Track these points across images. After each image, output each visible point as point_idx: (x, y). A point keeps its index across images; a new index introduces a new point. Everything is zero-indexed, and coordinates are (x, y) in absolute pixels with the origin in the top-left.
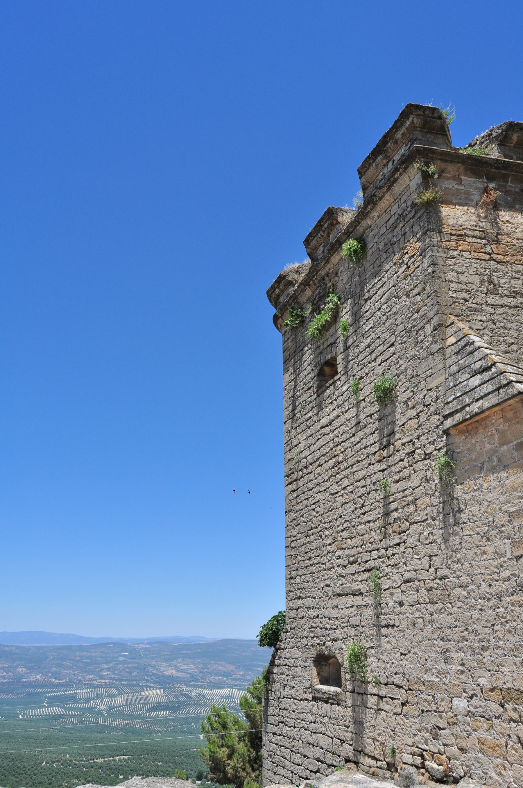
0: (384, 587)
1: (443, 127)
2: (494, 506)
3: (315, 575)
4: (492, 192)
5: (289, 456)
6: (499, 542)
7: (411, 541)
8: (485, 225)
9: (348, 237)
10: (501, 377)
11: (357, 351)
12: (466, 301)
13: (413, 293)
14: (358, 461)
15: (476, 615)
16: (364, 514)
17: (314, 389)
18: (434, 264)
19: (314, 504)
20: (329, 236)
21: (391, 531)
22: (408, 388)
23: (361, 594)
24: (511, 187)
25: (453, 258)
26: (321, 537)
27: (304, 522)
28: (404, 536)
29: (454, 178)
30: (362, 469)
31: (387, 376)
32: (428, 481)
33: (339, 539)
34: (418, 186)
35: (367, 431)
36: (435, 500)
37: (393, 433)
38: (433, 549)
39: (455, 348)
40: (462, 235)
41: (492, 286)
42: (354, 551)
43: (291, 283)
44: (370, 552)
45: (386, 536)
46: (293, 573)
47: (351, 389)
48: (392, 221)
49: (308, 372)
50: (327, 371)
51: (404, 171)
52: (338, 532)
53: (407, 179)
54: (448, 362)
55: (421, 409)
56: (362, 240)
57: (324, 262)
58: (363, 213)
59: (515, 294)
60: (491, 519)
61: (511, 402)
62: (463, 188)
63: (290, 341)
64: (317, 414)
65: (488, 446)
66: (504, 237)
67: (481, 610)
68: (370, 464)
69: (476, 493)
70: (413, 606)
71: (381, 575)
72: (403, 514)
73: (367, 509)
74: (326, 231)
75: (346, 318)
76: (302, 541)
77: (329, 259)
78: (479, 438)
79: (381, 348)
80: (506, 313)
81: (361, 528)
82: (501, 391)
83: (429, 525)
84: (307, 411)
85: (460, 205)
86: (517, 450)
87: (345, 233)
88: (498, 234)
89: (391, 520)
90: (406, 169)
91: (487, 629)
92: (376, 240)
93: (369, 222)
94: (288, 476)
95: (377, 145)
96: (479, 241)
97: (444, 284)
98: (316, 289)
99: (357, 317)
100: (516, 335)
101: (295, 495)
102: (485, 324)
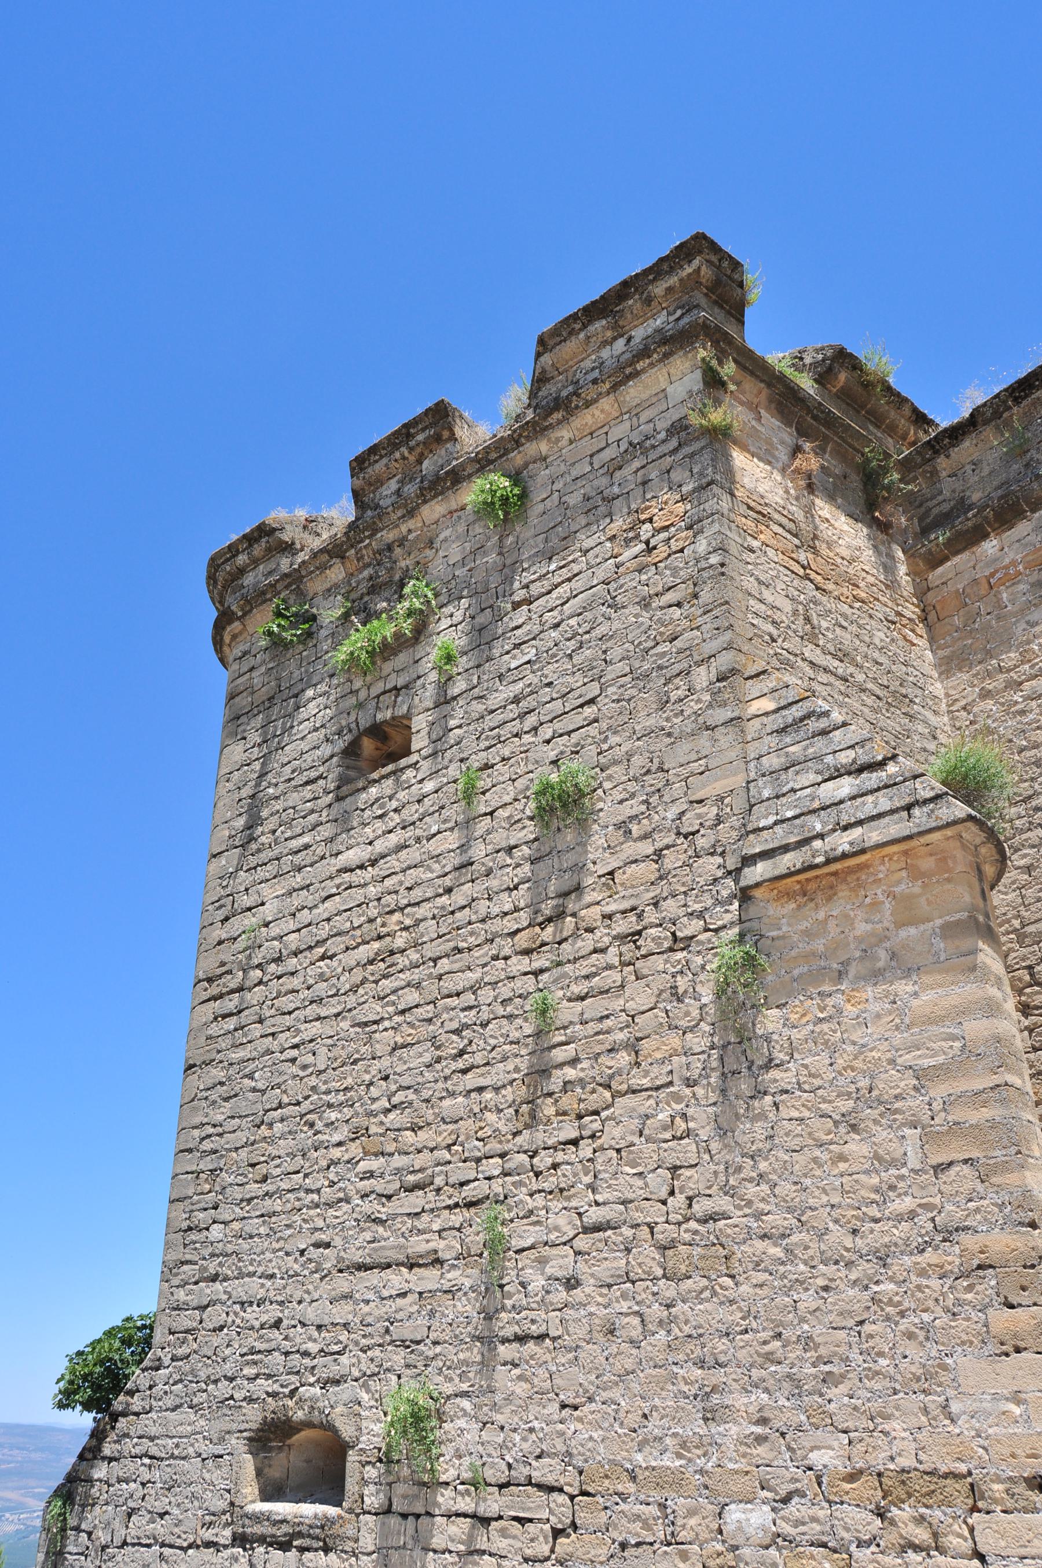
15: (808, 1300)
16: (464, 1071)
20: (420, 462)
26: (312, 1125)
40: (764, 516)
43: (288, 548)
51: (660, 361)
59: (842, 655)
60: (864, 1083)
67: (826, 1289)
70: (609, 1286)
74: (419, 450)
85: (760, 459)
86: (944, 937)
90: (666, 356)
91: (842, 1334)
93: (543, 447)
95: (602, 297)
96: (789, 536)
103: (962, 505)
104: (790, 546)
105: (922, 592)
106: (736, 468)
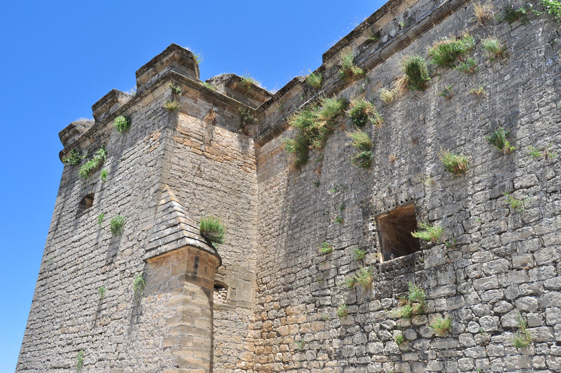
0: (85, 363)
1: (193, 65)
2: (160, 313)
3: (41, 352)
4: (213, 114)
5: (45, 259)
6: (157, 337)
7: (109, 332)
8: (205, 132)
9: (121, 114)
10: (181, 233)
11: (108, 193)
12: (180, 178)
13: (149, 164)
14: (90, 271)
16: (85, 309)
17: (75, 213)
18: (165, 149)
19: (54, 297)
20: (110, 108)
21: (98, 323)
22: (132, 227)
23: (69, 367)
24: (226, 113)
25: (179, 148)
26: (53, 323)
27: (44, 310)
28: (105, 328)
29: (193, 98)
30: (91, 277)
31: (121, 215)
32: (128, 292)
33: (65, 326)
34: (169, 96)
35: (101, 250)
36: (129, 306)
37: (115, 255)
38: (120, 339)
39: (163, 207)
40: (188, 136)
41: (199, 172)
42: (71, 336)
43: (77, 132)
44: (82, 337)
45: (95, 327)
46: (26, 349)
47: (98, 219)
48: (149, 113)
49: (74, 200)
50: (86, 202)
52: (65, 321)
53: (163, 90)
54: (158, 215)
55: (135, 242)
56: (129, 119)
57: (102, 125)
58: (133, 102)
59: (212, 180)
60: (156, 322)
61: (183, 249)
62: (197, 106)
63: (67, 173)
64: (72, 232)
65: (166, 275)
66: (214, 143)
68: (97, 275)
69: (153, 304)
71: (85, 355)
72: (108, 313)
73: (87, 306)
74: (109, 104)
75: (107, 168)
76: (38, 325)
77: (106, 124)
78: (162, 268)
79: (123, 196)
80: (204, 190)
81: (81, 320)
82: (179, 241)
83: (122, 322)
84: (66, 227)
85: (192, 116)
86: (179, 280)
87: (119, 111)
88: (211, 140)
89: (100, 316)
90: (164, 83)
92: (137, 122)
94: (41, 274)
96: (198, 141)
97: (169, 164)
98: (94, 142)
99: (114, 169)
100: (206, 205)
101: (43, 288)
102: (188, 195)
103: (269, 127)
104: (197, 145)
105: (257, 155)
106: (179, 121)
